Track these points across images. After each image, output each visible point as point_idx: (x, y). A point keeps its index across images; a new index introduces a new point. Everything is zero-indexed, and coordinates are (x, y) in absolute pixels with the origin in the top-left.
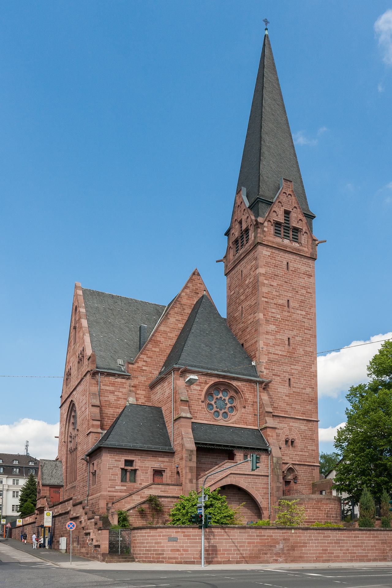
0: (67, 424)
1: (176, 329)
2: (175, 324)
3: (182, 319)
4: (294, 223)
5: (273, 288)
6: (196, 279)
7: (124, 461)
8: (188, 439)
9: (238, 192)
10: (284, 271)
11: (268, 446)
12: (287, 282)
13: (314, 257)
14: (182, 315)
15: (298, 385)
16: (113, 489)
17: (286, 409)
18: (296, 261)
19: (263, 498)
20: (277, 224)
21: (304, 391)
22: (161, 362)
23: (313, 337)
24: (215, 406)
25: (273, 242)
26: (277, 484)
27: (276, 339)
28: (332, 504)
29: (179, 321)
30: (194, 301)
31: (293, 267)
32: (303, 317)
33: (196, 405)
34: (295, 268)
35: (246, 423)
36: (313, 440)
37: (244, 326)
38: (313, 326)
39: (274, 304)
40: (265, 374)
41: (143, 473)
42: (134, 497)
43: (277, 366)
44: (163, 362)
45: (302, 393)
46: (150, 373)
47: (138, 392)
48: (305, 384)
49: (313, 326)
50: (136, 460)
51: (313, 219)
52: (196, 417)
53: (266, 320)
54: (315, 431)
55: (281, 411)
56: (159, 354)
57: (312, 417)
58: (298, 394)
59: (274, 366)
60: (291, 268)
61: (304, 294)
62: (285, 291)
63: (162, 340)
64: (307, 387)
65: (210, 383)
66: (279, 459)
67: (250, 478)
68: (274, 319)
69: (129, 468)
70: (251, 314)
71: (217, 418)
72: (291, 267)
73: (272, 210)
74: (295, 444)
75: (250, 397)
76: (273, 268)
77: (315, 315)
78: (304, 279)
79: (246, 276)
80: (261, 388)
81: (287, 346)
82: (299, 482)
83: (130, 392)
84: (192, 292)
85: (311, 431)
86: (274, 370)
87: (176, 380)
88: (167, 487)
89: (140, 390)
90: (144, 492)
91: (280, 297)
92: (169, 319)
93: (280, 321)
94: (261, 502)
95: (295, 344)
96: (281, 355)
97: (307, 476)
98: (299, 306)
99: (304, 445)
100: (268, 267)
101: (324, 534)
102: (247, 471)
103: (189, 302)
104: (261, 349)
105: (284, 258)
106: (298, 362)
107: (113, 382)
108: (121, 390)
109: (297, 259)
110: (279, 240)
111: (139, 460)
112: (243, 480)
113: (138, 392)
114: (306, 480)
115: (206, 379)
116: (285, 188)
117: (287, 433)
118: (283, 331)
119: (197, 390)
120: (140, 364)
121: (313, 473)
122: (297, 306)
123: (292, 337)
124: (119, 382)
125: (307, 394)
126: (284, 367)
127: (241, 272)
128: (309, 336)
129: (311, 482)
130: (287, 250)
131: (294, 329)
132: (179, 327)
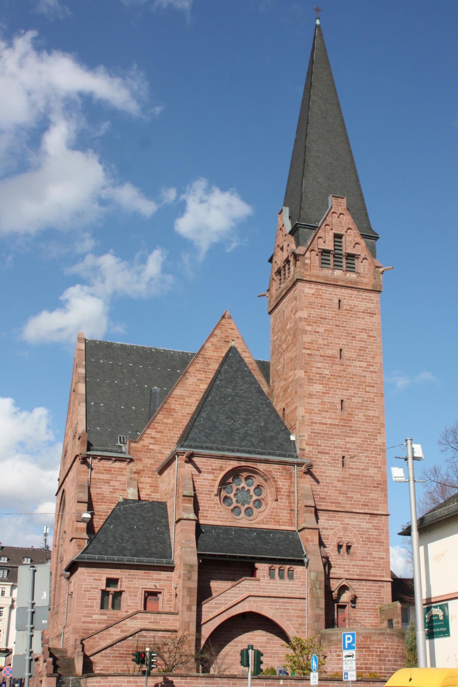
0: (60, 520)
1: (197, 391)
2: (196, 385)
3: (205, 378)
5: (319, 335)
6: (226, 323)
7: (105, 580)
8: (188, 549)
10: (335, 311)
11: (305, 556)
12: (339, 326)
13: (378, 290)
14: (206, 372)
16: (89, 619)
17: (338, 500)
18: (351, 297)
19: (297, 632)
20: (325, 252)
23: (378, 396)
24: (234, 500)
25: (318, 277)
26: (317, 611)
27: (323, 403)
28: (388, 642)
29: (202, 380)
30: (223, 352)
31: (348, 305)
32: (363, 371)
33: (207, 500)
34: (351, 305)
35: (279, 522)
36: (380, 542)
39: (321, 356)
40: (306, 452)
41: (130, 596)
42: (112, 630)
43: (324, 440)
44: (177, 437)
45: (362, 476)
46: (160, 453)
47: (142, 479)
48: (367, 463)
50: (122, 578)
51: (376, 240)
52: (207, 517)
53: (308, 379)
54: (383, 530)
55: (331, 503)
56: (172, 427)
57: (378, 510)
58: (357, 477)
59: (320, 440)
61: (364, 338)
63: (177, 407)
64: (371, 467)
65: (227, 470)
66: (319, 574)
67: (279, 602)
68: (319, 377)
69: (112, 589)
70: (292, 370)
71: (239, 515)
72: (345, 305)
74: (352, 550)
75: (285, 485)
76: (318, 309)
78: (364, 318)
79: (287, 319)
80: (301, 471)
81: (339, 411)
82: (358, 605)
83: (130, 481)
84: (221, 341)
85: (377, 529)
86: (320, 446)
87: (180, 467)
88: (158, 617)
89: (145, 477)
91: (329, 346)
92: (187, 379)
93: (328, 378)
95: (352, 408)
96: (330, 424)
97: (372, 598)
98: (357, 355)
99: (366, 550)
100: (312, 308)
102: (273, 592)
103: (215, 354)
106: (355, 432)
107: (109, 467)
109: (353, 294)
110: (327, 272)
111: (126, 578)
112: (268, 605)
113: (142, 479)
115: (221, 464)
116: (334, 207)
118: (333, 391)
119: (209, 480)
120: (146, 441)
121: (381, 593)
122: (355, 356)
123: (347, 399)
124: (116, 468)
125: (370, 477)
126: (334, 441)
127: (283, 312)
128: (372, 395)
129: (378, 607)
130: (339, 283)
131: (350, 387)
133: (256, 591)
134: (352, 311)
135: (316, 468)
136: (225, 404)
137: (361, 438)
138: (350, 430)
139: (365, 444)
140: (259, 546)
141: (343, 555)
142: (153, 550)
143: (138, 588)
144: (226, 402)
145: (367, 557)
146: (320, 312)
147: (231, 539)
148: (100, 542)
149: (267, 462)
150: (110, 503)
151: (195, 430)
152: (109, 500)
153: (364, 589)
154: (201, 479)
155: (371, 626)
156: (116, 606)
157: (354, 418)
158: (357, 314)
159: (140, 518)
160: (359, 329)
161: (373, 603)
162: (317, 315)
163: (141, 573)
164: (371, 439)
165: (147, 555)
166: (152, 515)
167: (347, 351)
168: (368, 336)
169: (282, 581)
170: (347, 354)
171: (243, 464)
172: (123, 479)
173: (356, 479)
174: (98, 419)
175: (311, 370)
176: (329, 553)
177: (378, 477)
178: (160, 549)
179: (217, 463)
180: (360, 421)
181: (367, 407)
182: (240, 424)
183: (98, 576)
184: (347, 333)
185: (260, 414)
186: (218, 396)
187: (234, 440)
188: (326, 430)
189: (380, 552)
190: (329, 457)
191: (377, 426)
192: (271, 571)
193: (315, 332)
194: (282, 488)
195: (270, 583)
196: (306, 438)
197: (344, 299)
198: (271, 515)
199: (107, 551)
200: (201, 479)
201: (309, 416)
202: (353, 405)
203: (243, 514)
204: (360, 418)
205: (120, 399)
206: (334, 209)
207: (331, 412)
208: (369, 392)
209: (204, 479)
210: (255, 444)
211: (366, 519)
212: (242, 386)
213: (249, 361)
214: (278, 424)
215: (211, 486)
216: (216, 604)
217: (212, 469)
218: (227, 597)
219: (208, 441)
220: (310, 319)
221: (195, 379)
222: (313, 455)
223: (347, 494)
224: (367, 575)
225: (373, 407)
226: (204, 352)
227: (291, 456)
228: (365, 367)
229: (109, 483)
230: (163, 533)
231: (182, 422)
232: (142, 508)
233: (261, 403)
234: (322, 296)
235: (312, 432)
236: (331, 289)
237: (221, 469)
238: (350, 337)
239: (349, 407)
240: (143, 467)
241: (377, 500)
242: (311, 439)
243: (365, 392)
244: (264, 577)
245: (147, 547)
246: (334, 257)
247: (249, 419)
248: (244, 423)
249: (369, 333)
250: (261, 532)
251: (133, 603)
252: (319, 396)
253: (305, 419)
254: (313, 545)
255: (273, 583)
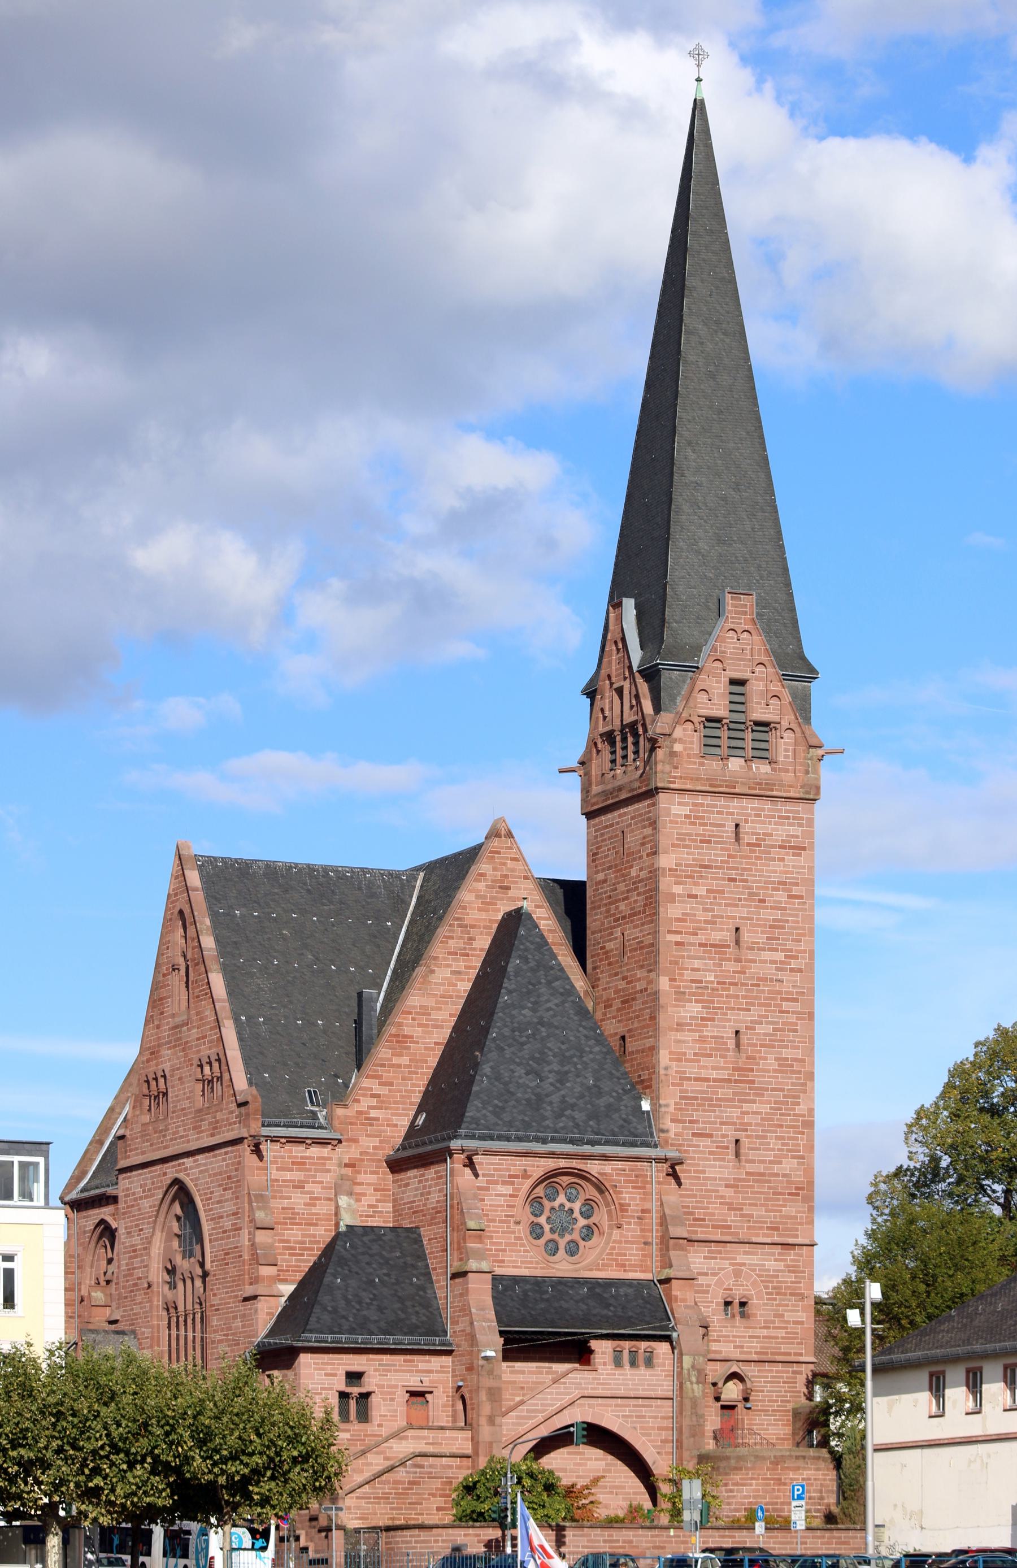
1: (451, 997)
2: (449, 985)
3: (466, 967)
4: (758, 714)
9: (615, 603)
12: (733, 880)
14: (467, 955)
15: (759, 1155)
17: (726, 1221)
18: (760, 816)
19: (658, 1453)
21: (776, 1168)
22: (414, 1092)
23: (804, 1019)
24: (547, 1228)
27: (703, 1040)
28: (810, 1469)
29: (459, 973)
31: (753, 834)
33: (503, 1232)
35: (624, 1265)
37: (627, 989)
38: (804, 988)
39: (700, 945)
40: (672, 1135)
43: (703, 1111)
44: (419, 1092)
46: (388, 1125)
47: (360, 1178)
48: (779, 1150)
49: (804, 988)
52: (503, 1261)
53: (676, 993)
54: (803, 1272)
55: (714, 1227)
56: (410, 1073)
57: (796, 1236)
59: (697, 1110)
60: (746, 839)
61: (780, 902)
62: (730, 905)
63: (417, 1032)
64: (786, 1156)
67: (629, 1406)
68: (697, 988)
69: (355, 1391)
72: (747, 833)
73: (697, 689)
76: (696, 848)
77: (812, 957)
78: (783, 860)
84: (493, 887)
85: (793, 1272)
86: (697, 1122)
88: (440, 1434)
89: (365, 1173)
90: (392, 1448)
91: (715, 923)
92: (433, 972)
93: (713, 989)
94: (654, 1463)
95: (755, 1045)
96: (715, 1080)
97: (781, 1391)
98: (768, 938)
100: (685, 846)
101: (734, 1537)
102: (620, 1389)
103: (483, 915)
104: (662, 1072)
105: (728, 813)
106: (760, 1092)
107: (302, 1157)
108: (319, 1177)
109: (763, 810)
111: (375, 1370)
112: (612, 1411)
113: (360, 1178)
114: (777, 1401)
115: (526, 1165)
116: (732, 618)
117: (731, 1282)
119: (505, 1195)
120: (365, 1103)
121: (796, 1383)
123: (747, 1028)
124: (312, 1158)
125: (784, 1175)
126: (722, 1111)
128: (792, 1018)
129: (790, 1406)
130: (737, 790)
131: (753, 1004)
132: (459, 991)
133: (592, 1389)
134: (759, 845)
135: (689, 1165)
136: (523, 1044)
137: (769, 1102)
138: (750, 1089)
139: (776, 1114)
140: (595, 1312)
141: (733, 1316)
142: (414, 1321)
143: (396, 1386)
144: (524, 1039)
145: (774, 1322)
146: (699, 854)
147: (547, 1300)
148: (325, 1309)
149: (605, 1158)
150: (306, 1224)
151: (476, 1102)
152: (304, 1219)
153: (767, 1377)
154: (491, 1195)
155: (777, 1439)
156: (364, 1416)
157: (758, 1064)
158: (769, 853)
159: (381, 1261)
160: (774, 882)
161: (782, 1401)
162: (694, 860)
163: (400, 1361)
164: (787, 1103)
165: (405, 1330)
166: (398, 1254)
167: (749, 931)
168: (790, 897)
169: (635, 1371)
170: (748, 937)
171: (562, 1163)
172: (328, 1178)
173: (758, 1181)
174: (261, 1053)
175: (682, 975)
176: (709, 1317)
177: (799, 1176)
178: (424, 1318)
179: (518, 1164)
180: (768, 1071)
181: (783, 1041)
182: (552, 1084)
183: (331, 1369)
184: (750, 894)
185: (584, 1059)
186: (507, 1026)
187: (544, 1118)
188: (707, 1092)
189: (798, 1311)
190: (712, 1142)
191: (800, 1078)
192: (618, 1354)
193: (690, 896)
194: (629, 1205)
195: (614, 1375)
196: (672, 1109)
197: (746, 821)
198: (611, 1254)
199: (340, 1325)
200: (491, 1195)
201: (677, 1066)
202: (757, 1040)
203: (562, 1251)
204: (770, 1064)
205: (291, 1002)
206: (732, 623)
207: (716, 1056)
208: (788, 1012)
209: (497, 1195)
210: (581, 1123)
211: (773, 1254)
212: (548, 1001)
213: (549, 925)
214: (619, 1079)
215: (508, 1206)
216: (528, 1411)
217: (510, 1176)
218: (546, 1399)
219: (500, 1122)
220: (681, 870)
221: (446, 973)
222: (683, 1140)
223: (742, 1209)
224: (772, 1354)
225: (794, 1042)
226: (462, 913)
227: (647, 1145)
228: (782, 962)
229: (304, 1187)
230: (423, 1288)
231: (426, 1061)
232: (380, 1242)
233: (586, 1036)
234: (703, 818)
235: (681, 1098)
236: (721, 802)
237: (525, 1175)
238: (754, 901)
239: (749, 1045)
240: (361, 1153)
241: (796, 1217)
242: (681, 1109)
243: (781, 1012)
244: (605, 1364)
245: (403, 1316)
246: (729, 729)
247: (567, 1073)
248: (558, 1081)
249: (791, 890)
250: (594, 1284)
251: (389, 1411)
252: (696, 1025)
253: (669, 1072)
254: (686, 1307)
255: (619, 1375)
